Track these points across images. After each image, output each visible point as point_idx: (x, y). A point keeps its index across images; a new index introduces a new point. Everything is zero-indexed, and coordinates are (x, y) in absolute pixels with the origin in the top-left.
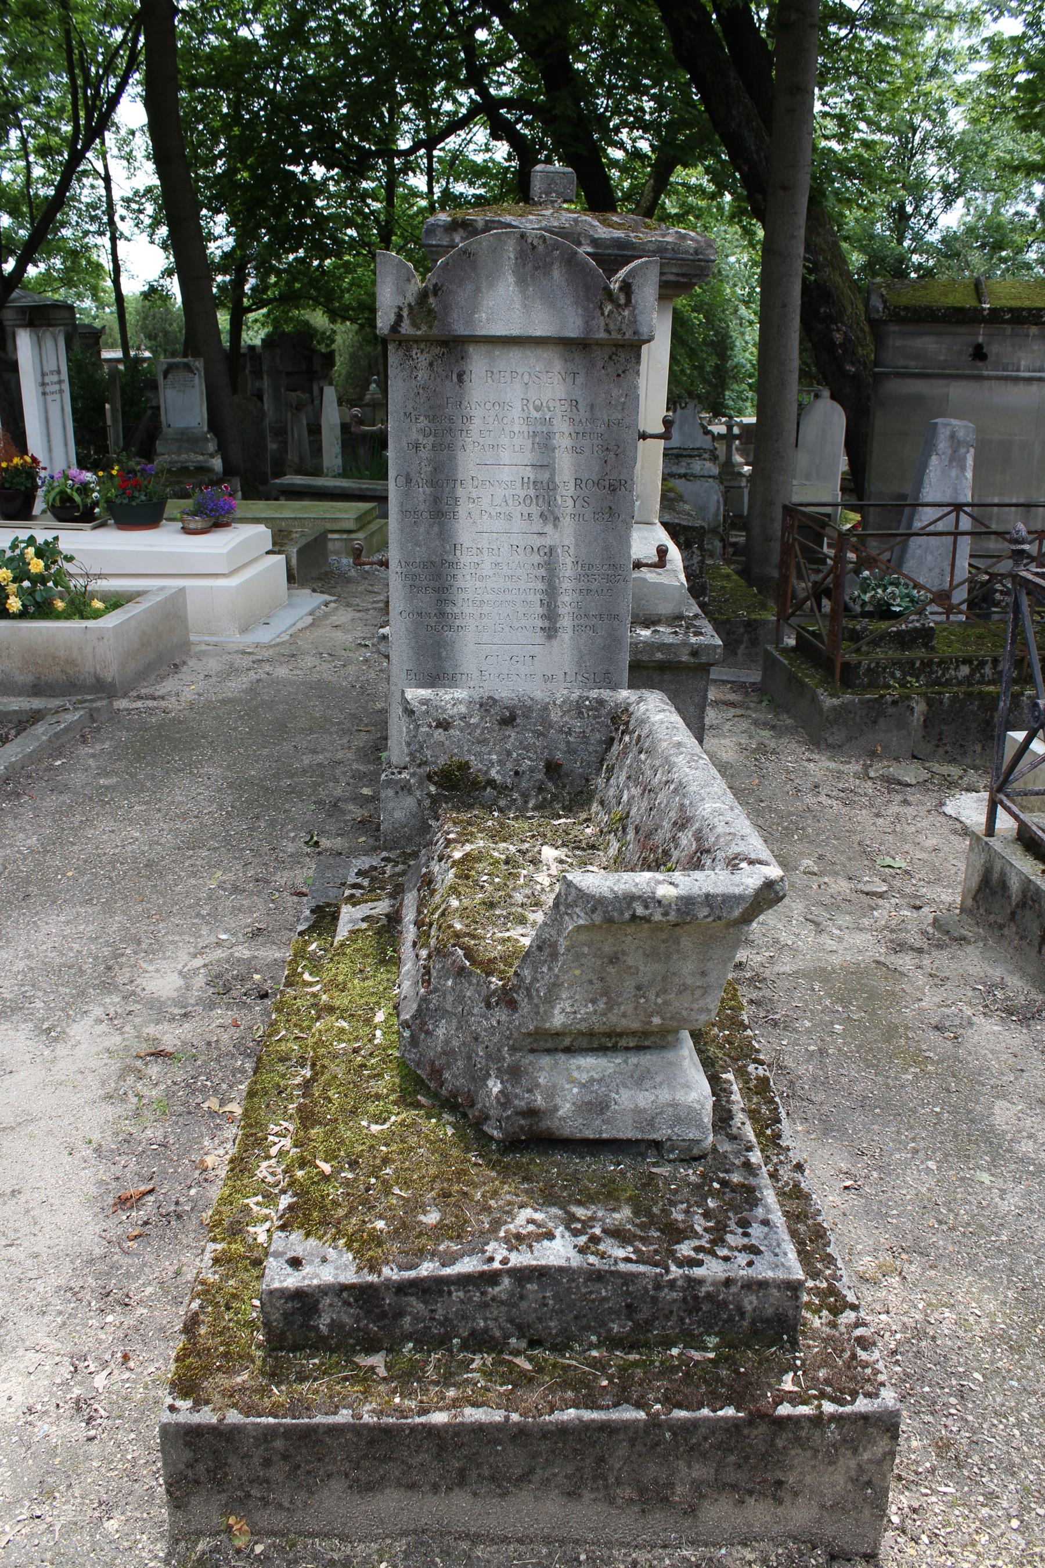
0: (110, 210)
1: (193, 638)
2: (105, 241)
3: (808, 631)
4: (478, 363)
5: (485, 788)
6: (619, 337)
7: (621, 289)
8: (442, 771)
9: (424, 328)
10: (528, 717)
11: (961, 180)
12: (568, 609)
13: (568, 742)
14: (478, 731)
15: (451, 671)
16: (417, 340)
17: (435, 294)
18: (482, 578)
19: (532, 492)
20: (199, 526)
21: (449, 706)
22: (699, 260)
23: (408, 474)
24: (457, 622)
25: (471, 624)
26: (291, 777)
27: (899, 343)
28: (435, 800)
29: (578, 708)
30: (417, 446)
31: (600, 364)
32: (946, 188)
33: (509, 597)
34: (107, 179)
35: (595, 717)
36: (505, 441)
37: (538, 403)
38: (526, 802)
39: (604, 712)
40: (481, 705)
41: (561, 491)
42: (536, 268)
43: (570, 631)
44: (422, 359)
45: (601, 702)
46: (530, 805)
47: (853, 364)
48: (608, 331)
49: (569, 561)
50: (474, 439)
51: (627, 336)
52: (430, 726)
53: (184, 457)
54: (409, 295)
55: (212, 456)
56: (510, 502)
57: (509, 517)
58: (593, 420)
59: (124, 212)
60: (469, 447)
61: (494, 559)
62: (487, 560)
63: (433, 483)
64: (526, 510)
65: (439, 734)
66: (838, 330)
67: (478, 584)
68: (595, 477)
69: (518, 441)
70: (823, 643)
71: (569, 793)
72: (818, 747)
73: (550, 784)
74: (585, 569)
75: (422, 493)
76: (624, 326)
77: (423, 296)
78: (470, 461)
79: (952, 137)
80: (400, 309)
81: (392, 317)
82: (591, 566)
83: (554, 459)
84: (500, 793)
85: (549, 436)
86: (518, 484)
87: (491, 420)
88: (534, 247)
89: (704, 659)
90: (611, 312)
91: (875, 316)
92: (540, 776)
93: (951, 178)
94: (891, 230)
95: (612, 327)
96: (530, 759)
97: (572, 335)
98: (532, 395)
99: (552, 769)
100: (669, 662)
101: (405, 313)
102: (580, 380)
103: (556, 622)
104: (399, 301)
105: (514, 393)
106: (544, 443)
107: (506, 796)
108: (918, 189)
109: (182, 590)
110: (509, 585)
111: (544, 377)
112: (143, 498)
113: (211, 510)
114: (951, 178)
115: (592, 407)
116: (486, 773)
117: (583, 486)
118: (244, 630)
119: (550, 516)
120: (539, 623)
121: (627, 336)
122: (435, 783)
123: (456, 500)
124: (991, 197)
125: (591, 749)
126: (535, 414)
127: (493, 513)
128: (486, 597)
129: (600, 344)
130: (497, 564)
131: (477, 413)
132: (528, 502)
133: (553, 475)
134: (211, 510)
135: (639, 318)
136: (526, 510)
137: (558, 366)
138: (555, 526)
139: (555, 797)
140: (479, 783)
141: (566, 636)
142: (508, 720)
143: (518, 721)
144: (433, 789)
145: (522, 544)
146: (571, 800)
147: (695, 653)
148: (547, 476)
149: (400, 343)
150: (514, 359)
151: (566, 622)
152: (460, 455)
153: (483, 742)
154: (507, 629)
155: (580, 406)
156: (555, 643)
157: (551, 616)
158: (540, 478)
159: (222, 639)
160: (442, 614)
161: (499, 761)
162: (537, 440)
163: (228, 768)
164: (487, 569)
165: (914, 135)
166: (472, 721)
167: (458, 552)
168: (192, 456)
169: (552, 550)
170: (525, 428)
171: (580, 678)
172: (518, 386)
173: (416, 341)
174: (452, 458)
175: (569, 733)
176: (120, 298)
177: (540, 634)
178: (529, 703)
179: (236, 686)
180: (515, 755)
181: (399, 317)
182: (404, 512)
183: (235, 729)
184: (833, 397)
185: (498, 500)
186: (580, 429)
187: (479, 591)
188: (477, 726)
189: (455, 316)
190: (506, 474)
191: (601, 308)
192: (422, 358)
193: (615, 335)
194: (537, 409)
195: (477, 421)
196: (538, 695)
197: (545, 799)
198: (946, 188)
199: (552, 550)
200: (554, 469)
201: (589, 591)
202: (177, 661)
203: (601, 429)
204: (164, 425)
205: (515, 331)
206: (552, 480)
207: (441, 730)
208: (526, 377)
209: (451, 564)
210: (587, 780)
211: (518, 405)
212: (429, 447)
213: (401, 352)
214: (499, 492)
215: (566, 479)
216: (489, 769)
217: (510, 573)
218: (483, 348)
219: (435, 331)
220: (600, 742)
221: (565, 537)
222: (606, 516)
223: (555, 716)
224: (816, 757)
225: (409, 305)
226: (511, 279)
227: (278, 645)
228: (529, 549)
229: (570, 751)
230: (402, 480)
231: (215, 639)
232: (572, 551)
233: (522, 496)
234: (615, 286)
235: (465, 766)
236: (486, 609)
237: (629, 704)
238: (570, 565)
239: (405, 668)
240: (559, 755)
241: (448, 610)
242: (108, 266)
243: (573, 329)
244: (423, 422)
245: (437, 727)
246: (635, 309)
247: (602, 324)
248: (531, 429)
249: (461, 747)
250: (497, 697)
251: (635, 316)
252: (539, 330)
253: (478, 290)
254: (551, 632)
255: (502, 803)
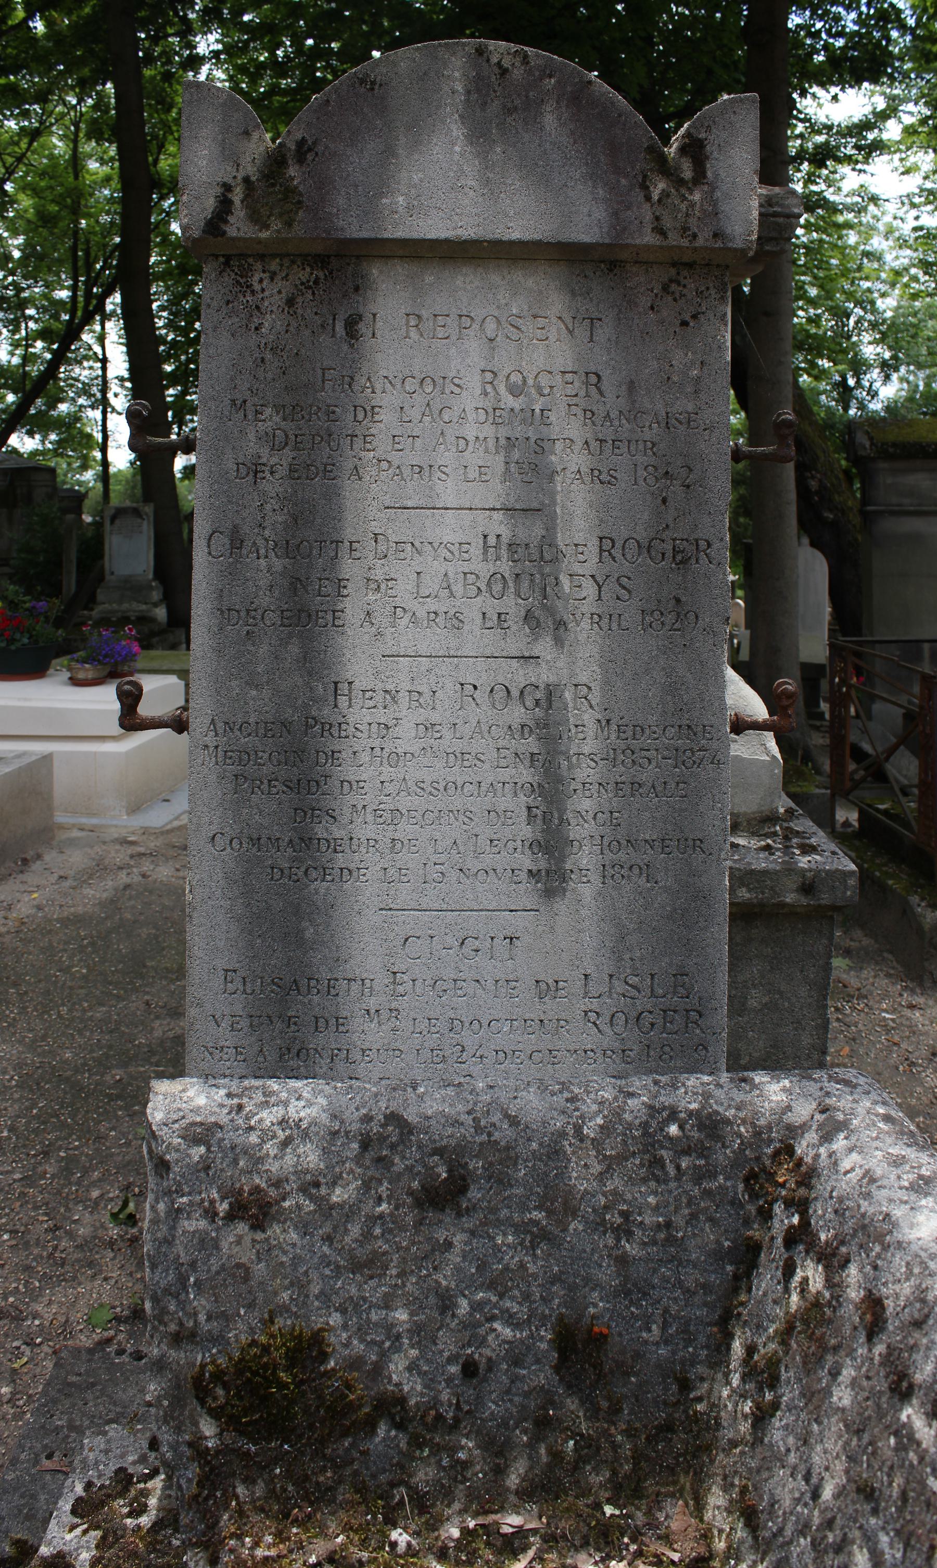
0: (104, 389)
1: (60, 818)
2: (97, 414)
3: (878, 810)
4: (390, 300)
5: (370, 1426)
6: (685, 243)
7: (683, 150)
8: (241, 1367)
9: (276, 224)
10: (503, 1181)
11: (894, 357)
12: (590, 828)
13: (623, 1261)
14: (355, 1230)
15: (325, 974)
16: (263, 254)
17: (301, 157)
18: (395, 759)
19: (505, 567)
20: (91, 675)
21: (270, 1148)
22: (775, 215)
23: (236, 529)
24: (341, 860)
25: (372, 864)
26: (125, 1065)
27: (889, 480)
28: (214, 1473)
29: (643, 1146)
30: (256, 470)
31: (645, 301)
32: (884, 365)
33: (458, 802)
34: (104, 361)
35: (699, 1176)
36: (446, 457)
37: (516, 378)
38: (499, 1471)
39: (722, 1156)
40: (365, 1145)
41: (570, 563)
42: (509, 111)
43: (595, 878)
44: (272, 292)
45: (711, 1125)
46: (513, 1480)
47: (831, 511)
48: (660, 231)
49: (589, 718)
50: (379, 453)
51: (700, 242)
52: (211, 1214)
53: (125, 606)
54: (246, 160)
55: (156, 605)
56: (458, 589)
57: (456, 621)
58: (633, 413)
59: (118, 390)
60: (370, 472)
61: (422, 715)
62: (409, 719)
63: (290, 548)
64: (492, 606)
65: (237, 1242)
66: (813, 477)
67: (387, 772)
68: (642, 534)
69: (474, 458)
70: (913, 833)
71: (630, 1433)
72: (921, 985)
73: (572, 1404)
74: (626, 737)
75: (264, 569)
76: (693, 222)
77: (276, 163)
78: (370, 502)
79: (884, 321)
80: (227, 188)
81: (210, 203)
82: (639, 729)
83: (553, 494)
84: (417, 1442)
85: (541, 446)
86: (476, 550)
87: (415, 414)
88: (504, 72)
89: (825, 899)
90: (665, 194)
91: (861, 453)
92: (541, 1376)
93: (887, 355)
94: (837, 401)
95: (667, 222)
96: (510, 1319)
97: (586, 239)
98: (505, 362)
99: (578, 1349)
100: (762, 905)
101: (237, 196)
102: (604, 332)
103: (562, 859)
104: (226, 173)
105: (466, 360)
106: (530, 462)
107: (436, 1450)
108: (859, 366)
109: (47, 759)
110: (457, 775)
111: (528, 326)
112: (26, 641)
113: (106, 656)
114: (887, 355)
115: (632, 387)
116: (378, 1371)
117: (617, 553)
118: (134, 809)
119: (546, 618)
120: (526, 861)
121: (700, 242)
122: (215, 1414)
123: (340, 584)
124: (921, 375)
125: (691, 1277)
126: (509, 401)
127: (421, 613)
128: (404, 802)
129: (643, 259)
130: (430, 727)
131: (387, 401)
132: (497, 588)
133: (551, 529)
134: (106, 656)
135: (724, 207)
136: (492, 606)
137: (557, 304)
138: (559, 642)
139: (589, 1448)
140: (352, 1407)
141: (585, 890)
142: (443, 1195)
143: (474, 1193)
144: (208, 1428)
145: (485, 682)
146: (637, 1457)
147: (808, 887)
148: (539, 531)
149: (228, 259)
150: (466, 292)
151: (585, 858)
152: (350, 490)
153: (367, 1265)
154: (454, 875)
155: (605, 385)
156: (562, 906)
157: (551, 843)
158: (522, 535)
159: (103, 822)
160: (305, 842)
161: (417, 1330)
162: (516, 455)
163: (32, 1046)
164: (406, 736)
165: (848, 319)
166: (338, 1195)
167: (343, 701)
168: (135, 605)
169: (550, 696)
170: (488, 431)
171: (619, 987)
172: (474, 345)
173: (262, 257)
174: (332, 495)
175: (624, 1231)
176: (105, 463)
177: (527, 885)
178: (504, 1133)
179: (96, 893)
180: (464, 1306)
181: (224, 205)
182: (225, 612)
183: (66, 970)
184: (813, 545)
185: (431, 584)
186: (608, 433)
187: (390, 788)
188: (349, 1212)
189: (341, 201)
190: (449, 529)
191: (645, 187)
192: (271, 289)
193: (674, 239)
194: (515, 391)
195: (387, 417)
196: (532, 1104)
197: (556, 1455)
198: (884, 365)
199: (550, 696)
200: (553, 517)
201: (636, 785)
202: (30, 854)
203: (653, 432)
204: (107, 572)
205: (467, 231)
206: (548, 540)
207: (242, 1228)
208: (491, 326)
209: (327, 728)
210: (685, 1385)
211: (474, 382)
212: (282, 471)
213: (228, 279)
214: (435, 567)
215: (579, 538)
216: (384, 1355)
217: (458, 746)
218: (401, 269)
219: (298, 230)
220: (719, 1256)
221: (579, 662)
222: (670, 618)
223: (582, 1174)
224: (920, 1000)
225: (246, 180)
226: (457, 131)
227: (172, 830)
228: (500, 694)
229: (631, 1289)
230: (222, 541)
231: (94, 821)
232: (595, 697)
233: (485, 575)
234: (672, 150)
235: (308, 1348)
236: (405, 829)
237: (794, 1131)
238: (591, 729)
239: (221, 963)
240: (597, 1305)
241: (320, 831)
242: (99, 437)
243: (587, 223)
244: (271, 419)
245: (231, 1217)
246: (713, 189)
247: (649, 217)
248: (503, 432)
249: (300, 1285)
250: (411, 1116)
251: (715, 203)
252: (517, 230)
253: (389, 151)
254: (551, 880)
255: (424, 1475)
